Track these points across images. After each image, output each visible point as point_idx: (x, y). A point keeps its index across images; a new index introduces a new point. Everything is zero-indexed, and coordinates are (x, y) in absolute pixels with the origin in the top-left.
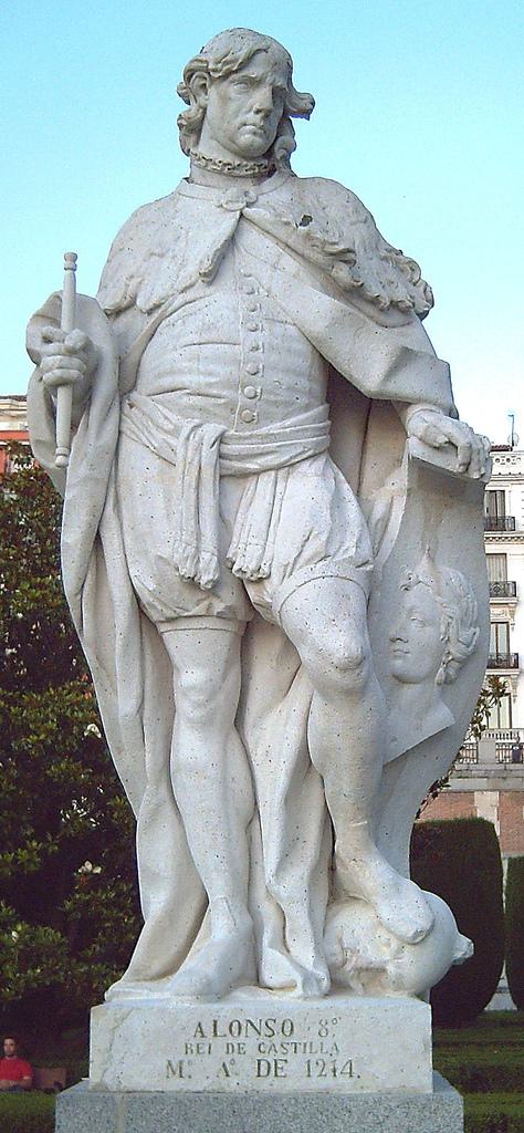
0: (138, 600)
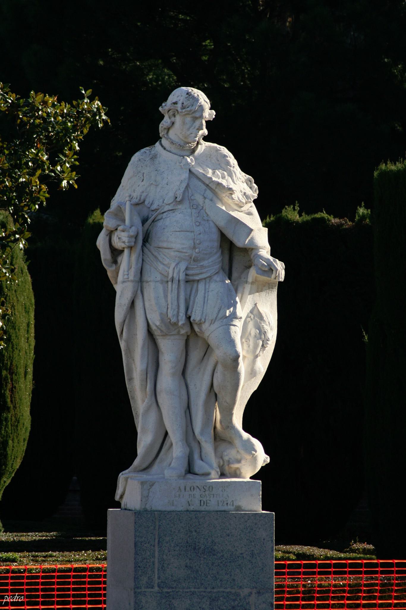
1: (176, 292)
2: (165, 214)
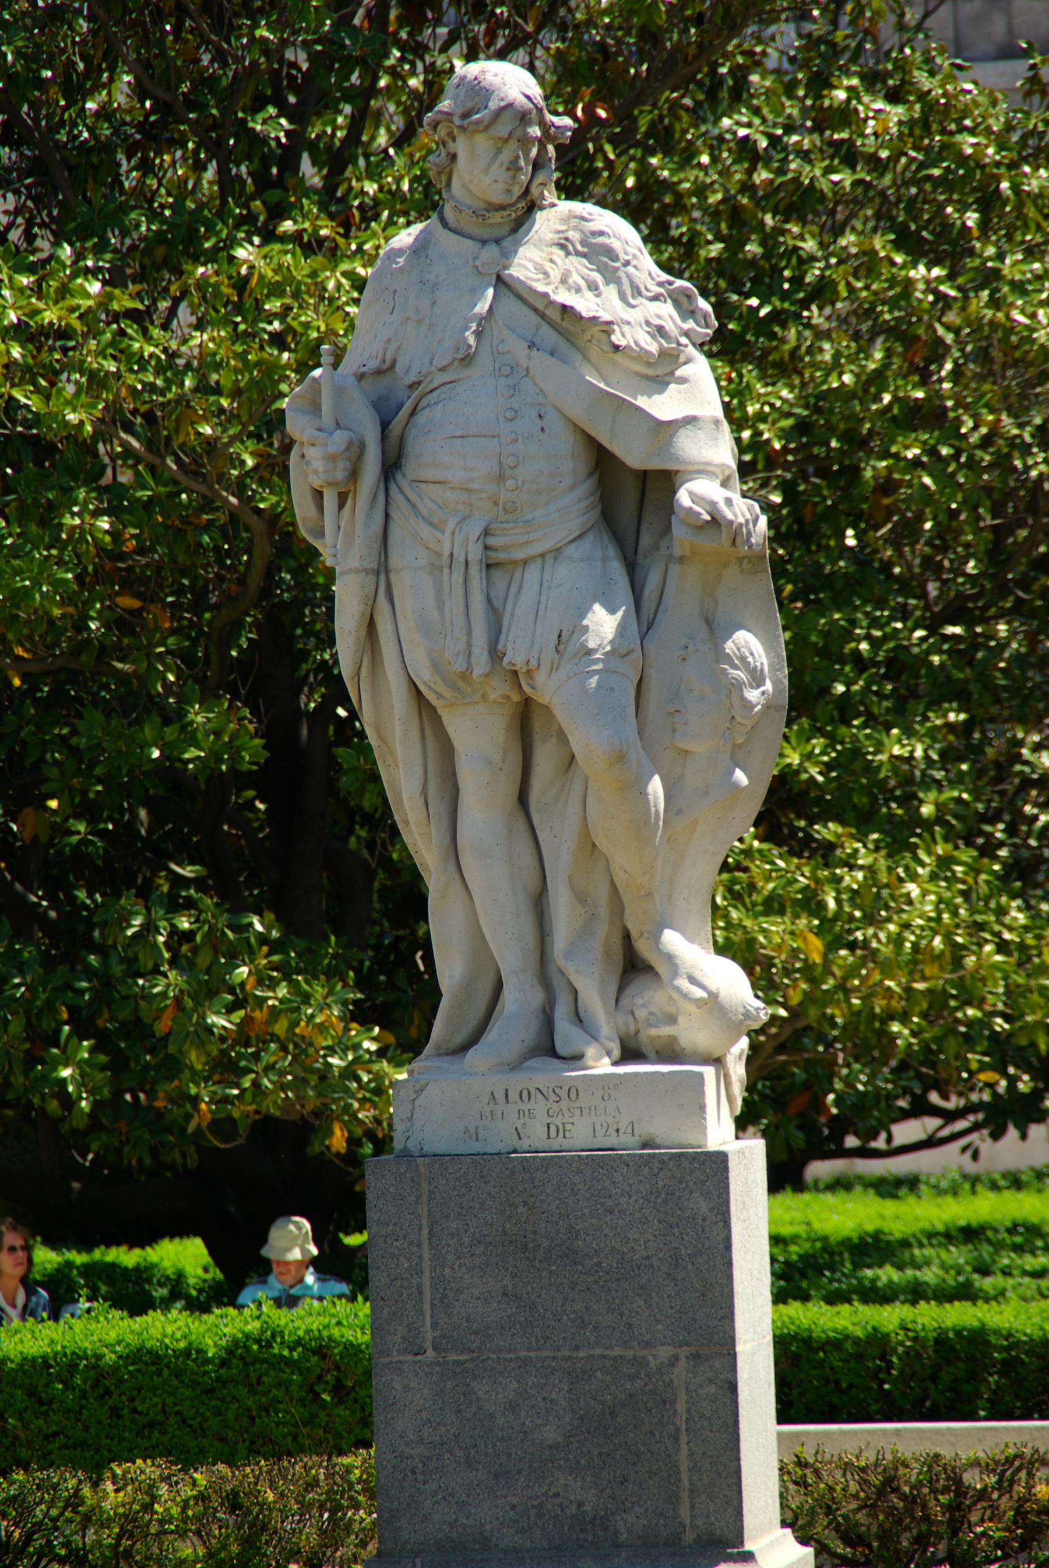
2: (435, 394)
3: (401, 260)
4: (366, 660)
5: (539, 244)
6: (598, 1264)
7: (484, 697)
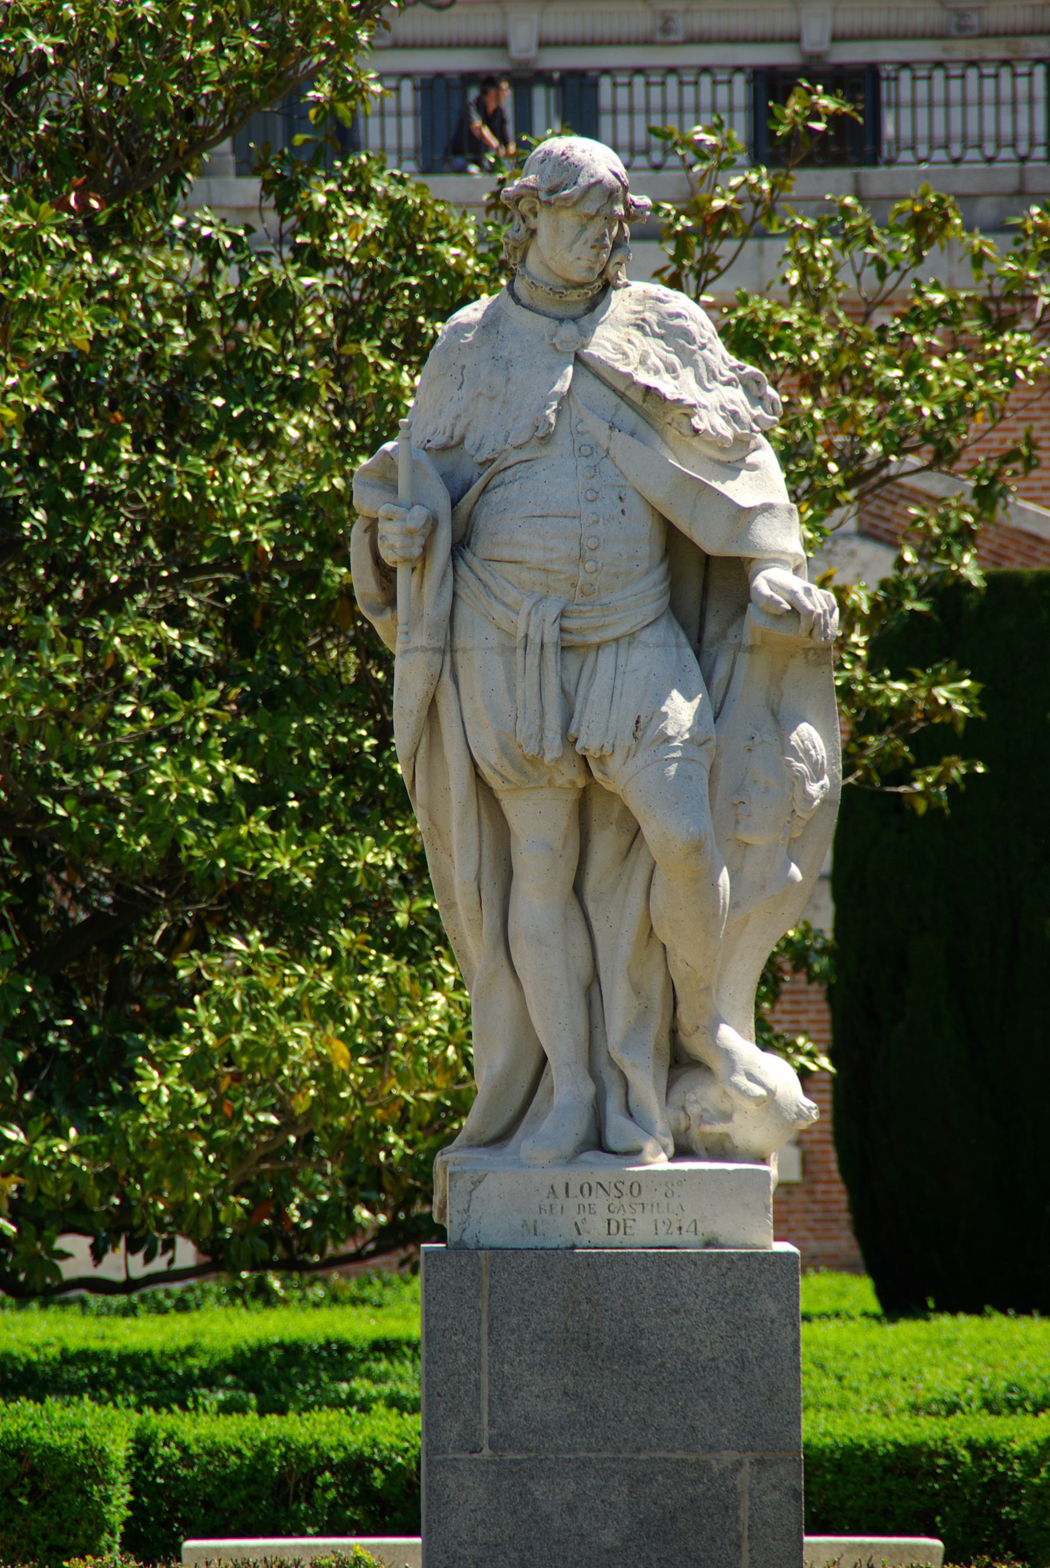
0: (475, 765)
1: (536, 675)
2: (509, 472)
3: (470, 336)
4: (424, 740)
5: (616, 324)
6: (663, 1365)
7: (550, 782)
